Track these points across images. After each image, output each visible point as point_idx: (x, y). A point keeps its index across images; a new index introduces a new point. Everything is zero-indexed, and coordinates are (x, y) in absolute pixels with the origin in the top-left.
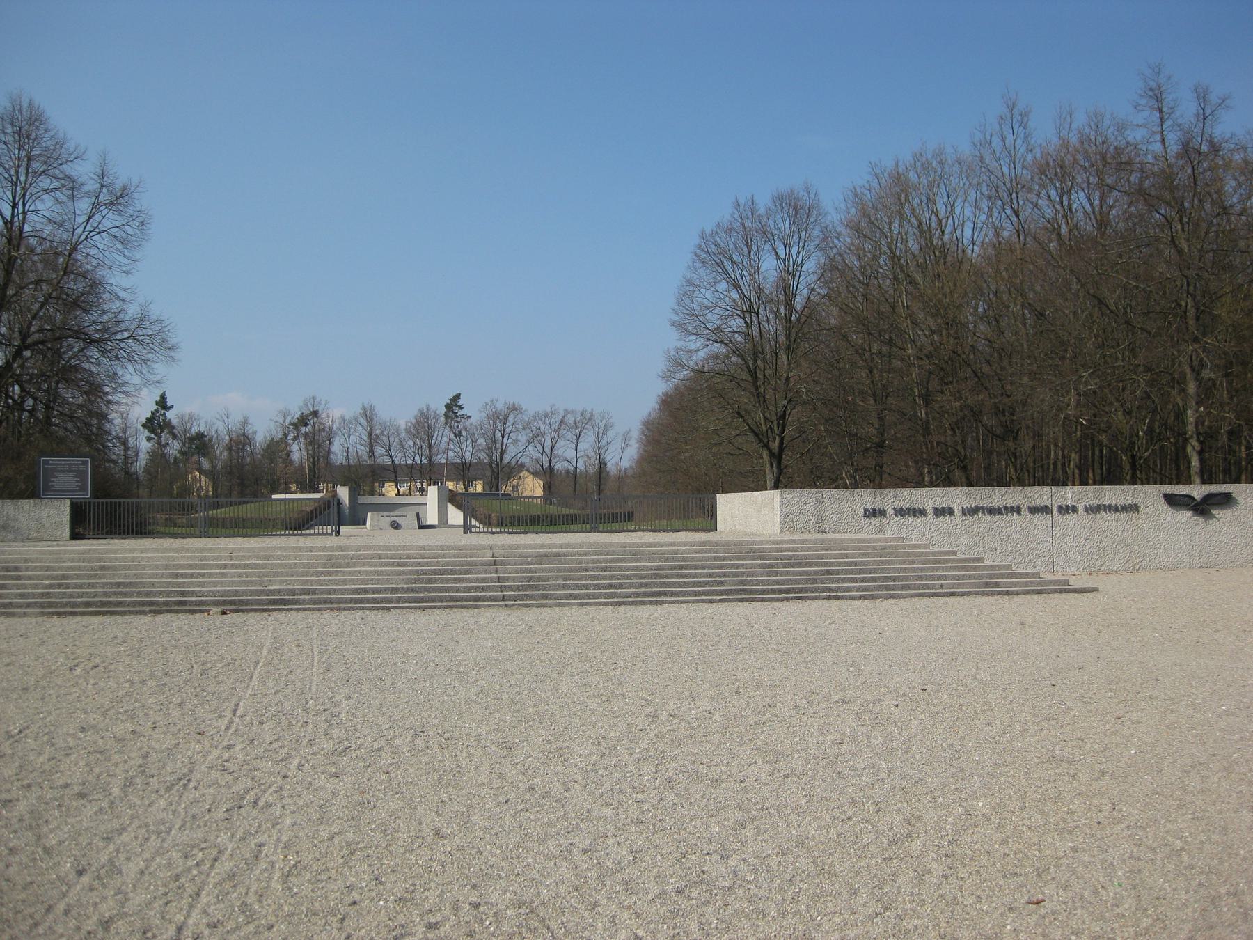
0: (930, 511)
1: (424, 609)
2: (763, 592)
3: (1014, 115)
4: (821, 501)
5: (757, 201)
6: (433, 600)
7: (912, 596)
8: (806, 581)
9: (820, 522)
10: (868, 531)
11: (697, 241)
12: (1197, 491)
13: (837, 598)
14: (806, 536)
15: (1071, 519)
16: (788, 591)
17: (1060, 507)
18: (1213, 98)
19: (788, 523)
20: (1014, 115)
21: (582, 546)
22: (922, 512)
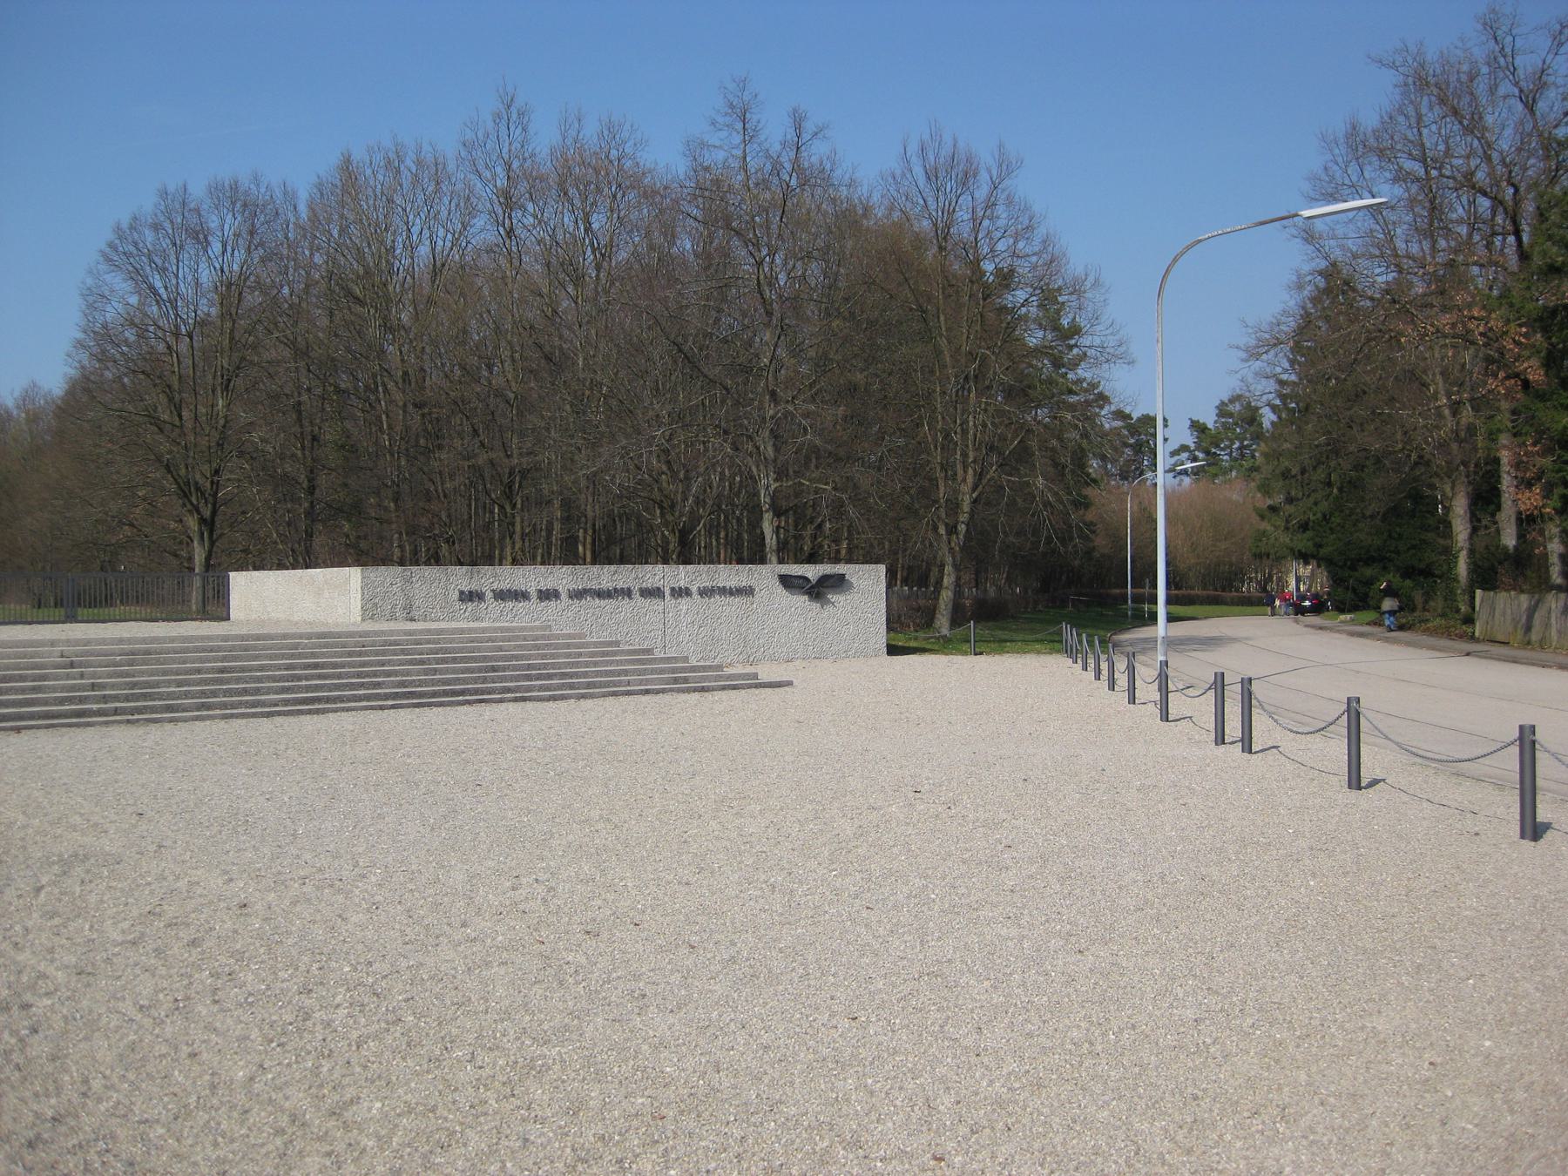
0: (534, 595)
1: (18, 730)
2: (434, 694)
3: (511, 114)
4: (409, 581)
5: (190, 189)
6: (32, 716)
7: (604, 695)
8: (475, 681)
9: (408, 608)
10: (464, 621)
11: (110, 236)
12: (812, 572)
13: (524, 699)
14: (393, 626)
15: (684, 603)
16: (462, 692)
17: (673, 589)
18: (809, 127)
19: (370, 610)
20: (511, 114)
21: (173, 640)
22: (524, 596)
